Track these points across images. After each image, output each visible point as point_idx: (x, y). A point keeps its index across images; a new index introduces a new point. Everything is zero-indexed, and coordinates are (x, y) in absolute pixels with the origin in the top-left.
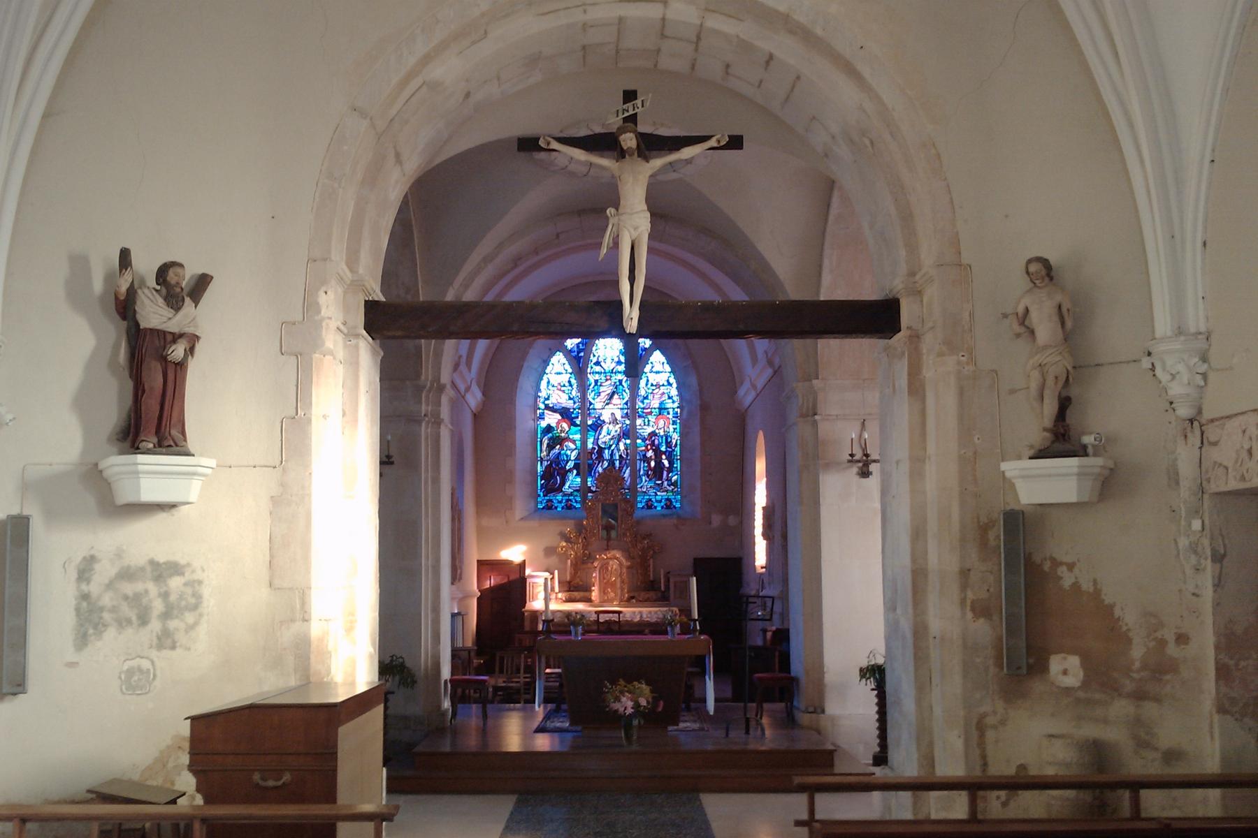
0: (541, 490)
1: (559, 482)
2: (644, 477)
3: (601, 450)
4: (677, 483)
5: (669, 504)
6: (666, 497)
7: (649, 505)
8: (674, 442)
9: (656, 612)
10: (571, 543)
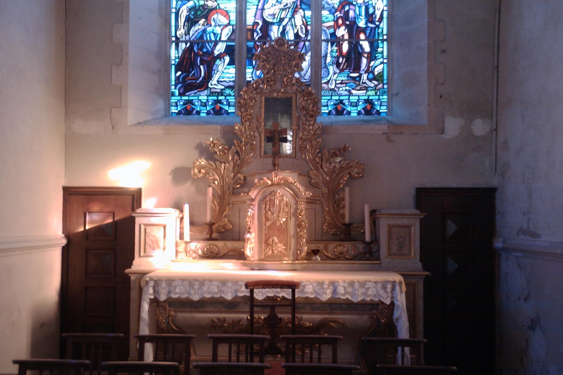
0: (176, 85)
1: (203, 74)
2: (331, 67)
3: (267, 25)
4: (383, 76)
5: (369, 107)
6: (366, 98)
7: (339, 109)
8: (378, 14)
9: (363, 284)
10: (215, 160)
